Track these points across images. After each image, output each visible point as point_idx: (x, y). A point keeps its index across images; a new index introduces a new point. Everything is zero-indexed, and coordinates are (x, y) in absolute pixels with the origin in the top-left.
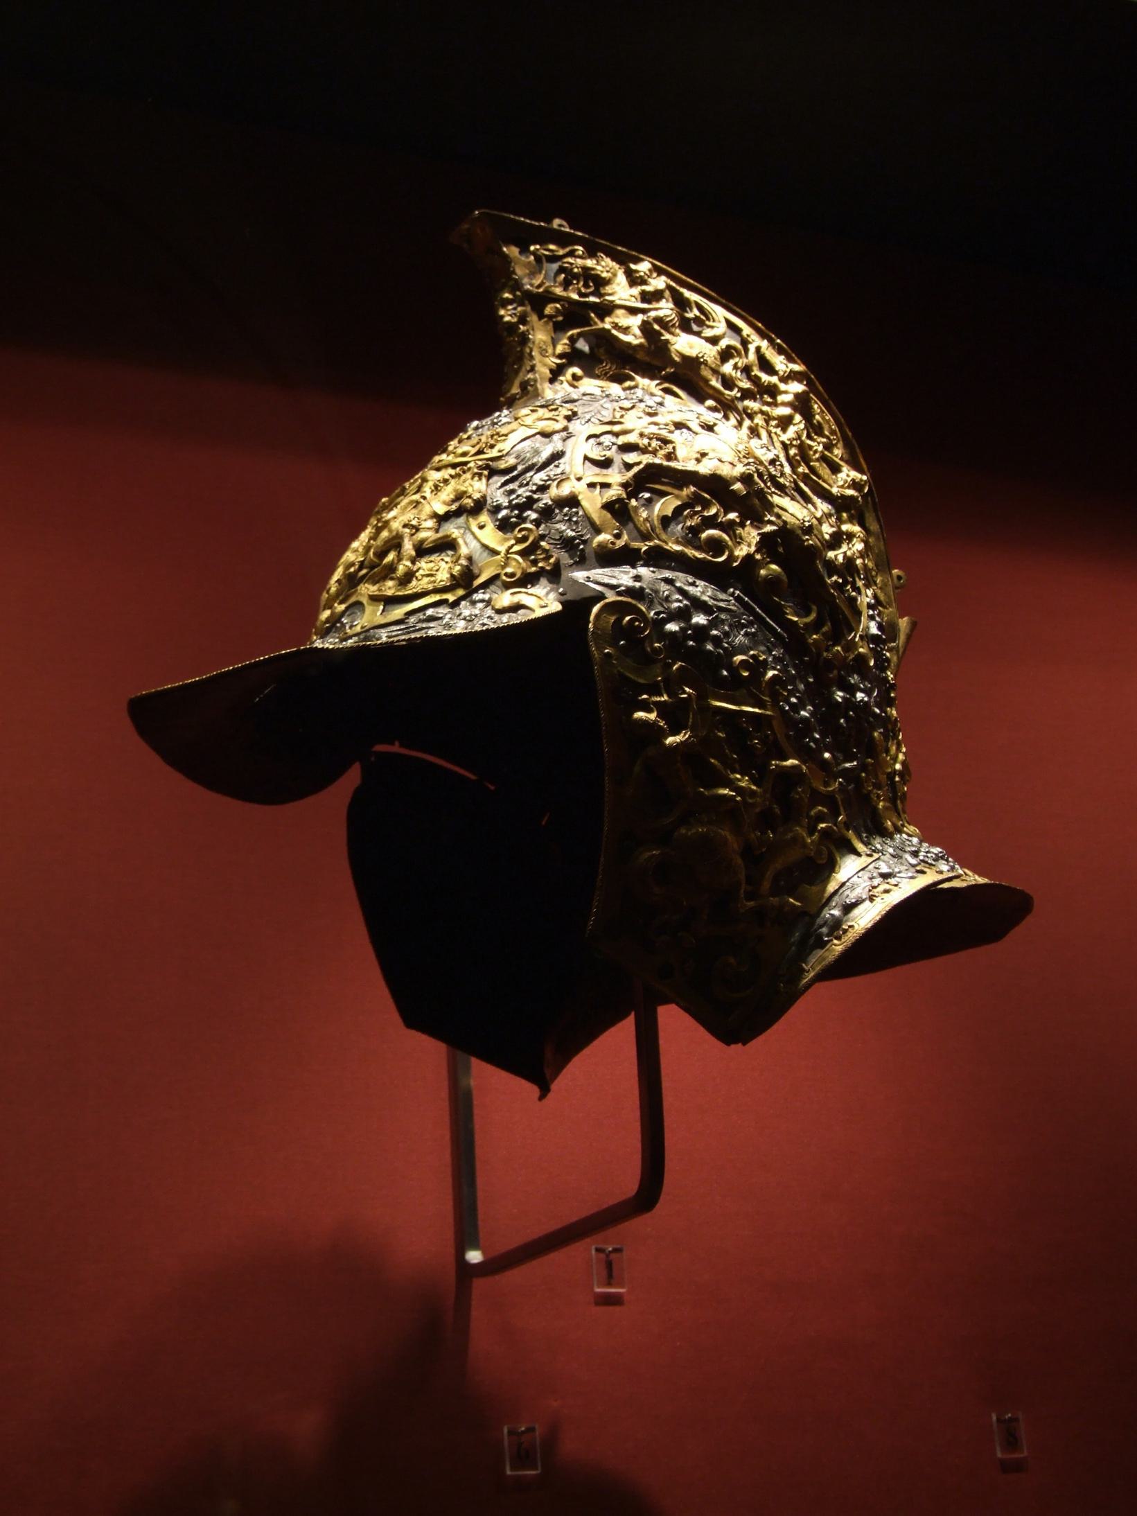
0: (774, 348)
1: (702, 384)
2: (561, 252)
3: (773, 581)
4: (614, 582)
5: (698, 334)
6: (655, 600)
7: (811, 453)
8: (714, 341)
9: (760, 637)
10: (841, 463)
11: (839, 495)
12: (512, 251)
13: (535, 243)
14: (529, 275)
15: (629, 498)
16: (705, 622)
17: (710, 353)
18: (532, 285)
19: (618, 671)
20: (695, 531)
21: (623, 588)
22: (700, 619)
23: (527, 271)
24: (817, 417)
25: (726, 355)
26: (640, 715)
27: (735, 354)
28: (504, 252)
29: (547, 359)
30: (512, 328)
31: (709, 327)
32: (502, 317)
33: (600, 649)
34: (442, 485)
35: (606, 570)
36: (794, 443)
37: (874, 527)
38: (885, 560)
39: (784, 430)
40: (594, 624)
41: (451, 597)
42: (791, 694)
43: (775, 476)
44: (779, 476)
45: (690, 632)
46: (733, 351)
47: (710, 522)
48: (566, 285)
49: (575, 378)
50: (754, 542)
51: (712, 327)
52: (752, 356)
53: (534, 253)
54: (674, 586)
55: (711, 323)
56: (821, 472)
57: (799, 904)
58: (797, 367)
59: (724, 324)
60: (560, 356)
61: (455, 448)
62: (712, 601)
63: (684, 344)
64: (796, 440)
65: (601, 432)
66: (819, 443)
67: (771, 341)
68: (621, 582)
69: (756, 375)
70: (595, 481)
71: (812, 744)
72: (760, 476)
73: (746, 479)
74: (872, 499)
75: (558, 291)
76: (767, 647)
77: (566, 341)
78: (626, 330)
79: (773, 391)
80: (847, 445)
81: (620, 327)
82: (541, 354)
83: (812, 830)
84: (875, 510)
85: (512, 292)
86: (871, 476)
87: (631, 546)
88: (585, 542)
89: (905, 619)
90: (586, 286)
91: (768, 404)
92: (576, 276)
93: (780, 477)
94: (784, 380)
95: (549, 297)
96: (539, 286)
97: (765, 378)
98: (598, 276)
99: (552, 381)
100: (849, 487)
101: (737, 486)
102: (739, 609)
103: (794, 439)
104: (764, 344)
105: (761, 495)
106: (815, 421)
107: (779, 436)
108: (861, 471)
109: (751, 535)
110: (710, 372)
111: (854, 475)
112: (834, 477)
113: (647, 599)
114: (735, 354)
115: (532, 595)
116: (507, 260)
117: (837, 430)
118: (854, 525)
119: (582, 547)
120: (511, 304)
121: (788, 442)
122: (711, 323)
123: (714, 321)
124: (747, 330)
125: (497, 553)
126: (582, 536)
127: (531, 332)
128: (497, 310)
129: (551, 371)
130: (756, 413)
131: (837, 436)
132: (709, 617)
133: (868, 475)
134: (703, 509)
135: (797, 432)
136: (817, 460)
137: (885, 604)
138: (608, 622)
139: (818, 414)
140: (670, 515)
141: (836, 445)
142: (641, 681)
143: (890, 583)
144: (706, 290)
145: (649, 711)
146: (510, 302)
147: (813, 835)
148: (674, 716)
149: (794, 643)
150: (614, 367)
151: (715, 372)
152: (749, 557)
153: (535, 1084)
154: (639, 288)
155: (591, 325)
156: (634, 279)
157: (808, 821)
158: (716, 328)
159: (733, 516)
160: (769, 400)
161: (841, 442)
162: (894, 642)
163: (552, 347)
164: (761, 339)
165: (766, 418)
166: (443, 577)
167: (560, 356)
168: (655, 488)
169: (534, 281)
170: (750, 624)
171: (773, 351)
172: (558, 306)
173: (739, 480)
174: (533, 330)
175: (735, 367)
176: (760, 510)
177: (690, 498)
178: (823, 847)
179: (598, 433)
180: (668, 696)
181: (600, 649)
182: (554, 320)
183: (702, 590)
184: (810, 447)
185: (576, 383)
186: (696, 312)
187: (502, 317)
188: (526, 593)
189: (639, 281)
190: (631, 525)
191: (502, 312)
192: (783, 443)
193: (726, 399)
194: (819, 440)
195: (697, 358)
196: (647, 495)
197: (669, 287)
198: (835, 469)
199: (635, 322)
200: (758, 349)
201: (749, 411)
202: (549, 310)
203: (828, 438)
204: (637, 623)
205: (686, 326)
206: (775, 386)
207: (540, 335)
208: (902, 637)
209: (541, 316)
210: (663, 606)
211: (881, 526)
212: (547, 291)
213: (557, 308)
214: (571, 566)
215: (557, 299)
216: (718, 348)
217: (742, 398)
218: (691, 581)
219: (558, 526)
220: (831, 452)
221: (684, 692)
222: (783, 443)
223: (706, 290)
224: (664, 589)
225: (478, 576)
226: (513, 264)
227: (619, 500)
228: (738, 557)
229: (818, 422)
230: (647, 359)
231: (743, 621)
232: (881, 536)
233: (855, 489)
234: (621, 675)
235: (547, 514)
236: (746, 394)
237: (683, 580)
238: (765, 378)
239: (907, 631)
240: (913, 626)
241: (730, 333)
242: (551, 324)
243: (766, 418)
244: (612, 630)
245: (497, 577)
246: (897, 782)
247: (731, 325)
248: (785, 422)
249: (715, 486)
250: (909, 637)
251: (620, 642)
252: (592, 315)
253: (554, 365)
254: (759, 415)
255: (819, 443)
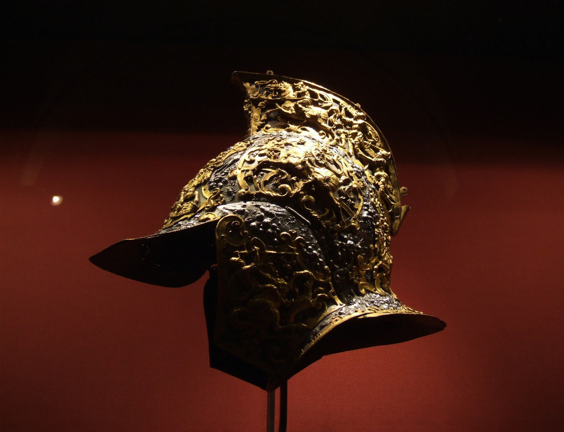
0: (353, 108)
1: (319, 125)
2: (267, 82)
3: (308, 202)
4: (233, 208)
5: (320, 106)
6: (249, 214)
7: (366, 146)
8: (326, 108)
9: (297, 224)
10: (380, 148)
11: (375, 161)
12: (247, 85)
13: (257, 81)
14: (253, 92)
15: (254, 175)
16: (269, 221)
17: (323, 113)
18: (253, 96)
19: (226, 243)
20: (276, 185)
21: (236, 211)
22: (267, 220)
23: (252, 91)
24: (370, 132)
25: (330, 114)
26: (233, 258)
27: (335, 112)
28: (244, 85)
29: (257, 123)
30: (247, 112)
31: (325, 103)
32: (244, 109)
33: (219, 235)
34: (201, 174)
35: (232, 204)
36: (357, 143)
37: (392, 171)
38: (397, 184)
39: (354, 139)
40: (218, 226)
41: (189, 216)
42: (310, 244)
43: (318, 161)
44: (320, 160)
45: (261, 225)
46: (334, 111)
47: (284, 182)
48: (267, 94)
49: (267, 128)
50: (300, 187)
51: (327, 103)
52: (343, 112)
53: (256, 85)
54: (260, 208)
55: (326, 102)
56: (370, 153)
57: (306, 326)
58: (362, 114)
59: (332, 101)
60: (262, 121)
61: (358, 142)
62: (275, 212)
63: (313, 111)
64: (358, 142)
65: (255, 150)
66: (370, 142)
67: (353, 106)
68: (236, 208)
69: (343, 119)
70: (244, 169)
71: (273, 270)
72: (310, 161)
73: (303, 163)
74: (392, 161)
75: (264, 97)
76: (299, 227)
77: (265, 115)
78: (288, 108)
79: (351, 124)
80: (383, 140)
81: (286, 108)
82: (255, 121)
83: (314, 296)
84: (394, 165)
85: (247, 100)
86: (392, 152)
87: (251, 193)
88: (235, 193)
89: (405, 206)
90: (275, 94)
91: (348, 129)
92: (271, 91)
93: (320, 161)
94: (356, 119)
95: (260, 100)
96: (256, 96)
97: (348, 119)
98: (280, 89)
99: (258, 131)
100: (381, 158)
101: (300, 166)
102: (288, 214)
103: (356, 142)
104: (349, 107)
105: (308, 169)
106: (368, 134)
107: (352, 141)
108: (388, 151)
109: (301, 184)
110: (322, 120)
111: (384, 152)
112: (376, 154)
113: (245, 214)
114: (335, 112)
115: (212, 214)
116: (245, 88)
117: (378, 136)
118: (382, 172)
119: (234, 195)
120: (247, 104)
121: (354, 143)
122: (326, 102)
123: (328, 100)
124: (342, 102)
125: (206, 199)
126: (235, 191)
127: (252, 114)
128: (243, 106)
129: (258, 127)
130: (341, 133)
131: (378, 138)
132: (271, 218)
133: (391, 152)
134: (282, 176)
135: (358, 139)
136: (369, 148)
137: (395, 201)
138: (225, 224)
139: (371, 131)
140: (268, 180)
141: (378, 141)
142: (236, 246)
143: (399, 192)
144: (326, 89)
145: (237, 257)
146: (246, 103)
147: (314, 298)
148: (248, 258)
149: (315, 225)
150: (283, 122)
151: (325, 120)
152: (297, 193)
153: (287, 383)
154: (297, 92)
155: (276, 108)
156: (295, 89)
157: (312, 294)
158: (328, 103)
159: (294, 178)
160: (349, 128)
161: (380, 140)
162: (399, 216)
163: (259, 118)
164: (348, 105)
165: (346, 134)
166: (189, 209)
167: (262, 121)
168: (266, 170)
169: (254, 95)
170: (293, 219)
171: (353, 109)
172: (263, 102)
173: (300, 164)
174: (253, 112)
175: (335, 117)
176: (307, 174)
177: (278, 173)
178: (320, 303)
179: (253, 150)
180: (248, 251)
181: (219, 235)
182: (262, 108)
183: (272, 208)
184: (365, 144)
185: (266, 130)
186: (320, 98)
187: (244, 109)
188: (211, 213)
189: (297, 89)
190: (253, 185)
191: (244, 107)
192: (352, 143)
193: (328, 130)
194: (369, 141)
195: (317, 115)
196: (262, 173)
197: (308, 90)
198: (376, 151)
199: (292, 105)
200: (346, 109)
201: (339, 133)
202: (260, 104)
203: (374, 139)
204: (237, 224)
205: (316, 104)
206: (352, 122)
207: (255, 114)
208: (402, 213)
209: (257, 107)
210: (252, 216)
211: (396, 171)
212: (259, 98)
213: (263, 103)
214: (230, 201)
215: (263, 100)
216: (328, 111)
217: (336, 128)
218: (267, 205)
219: (227, 188)
220: (375, 145)
221: (254, 248)
222: (352, 143)
223: (326, 89)
224: (254, 209)
225: (199, 208)
226: (247, 89)
227: (250, 176)
228: (292, 194)
229: (370, 134)
230: (296, 118)
231: (289, 219)
232: (395, 175)
233: (383, 158)
234: (227, 244)
235: (225, 183)
236: (339, 126)
237: (265, 205)
238: (348, 119)
239: (405, 210)
240: (408, 209)
241: (334, 104)
242: (260, 109)
243: (346, 134)
244: (226, 227)
245: (204, 208)
246: (374, 273)
247: (335, 101)
248: (354, 135)
249: (290, 167)
250: (406, 213)
251: (230, 231)
252: (277, 104)
253: (260, 124)
254: (343, 134)
255: (370, 142)
